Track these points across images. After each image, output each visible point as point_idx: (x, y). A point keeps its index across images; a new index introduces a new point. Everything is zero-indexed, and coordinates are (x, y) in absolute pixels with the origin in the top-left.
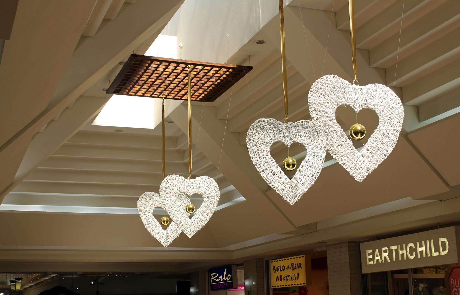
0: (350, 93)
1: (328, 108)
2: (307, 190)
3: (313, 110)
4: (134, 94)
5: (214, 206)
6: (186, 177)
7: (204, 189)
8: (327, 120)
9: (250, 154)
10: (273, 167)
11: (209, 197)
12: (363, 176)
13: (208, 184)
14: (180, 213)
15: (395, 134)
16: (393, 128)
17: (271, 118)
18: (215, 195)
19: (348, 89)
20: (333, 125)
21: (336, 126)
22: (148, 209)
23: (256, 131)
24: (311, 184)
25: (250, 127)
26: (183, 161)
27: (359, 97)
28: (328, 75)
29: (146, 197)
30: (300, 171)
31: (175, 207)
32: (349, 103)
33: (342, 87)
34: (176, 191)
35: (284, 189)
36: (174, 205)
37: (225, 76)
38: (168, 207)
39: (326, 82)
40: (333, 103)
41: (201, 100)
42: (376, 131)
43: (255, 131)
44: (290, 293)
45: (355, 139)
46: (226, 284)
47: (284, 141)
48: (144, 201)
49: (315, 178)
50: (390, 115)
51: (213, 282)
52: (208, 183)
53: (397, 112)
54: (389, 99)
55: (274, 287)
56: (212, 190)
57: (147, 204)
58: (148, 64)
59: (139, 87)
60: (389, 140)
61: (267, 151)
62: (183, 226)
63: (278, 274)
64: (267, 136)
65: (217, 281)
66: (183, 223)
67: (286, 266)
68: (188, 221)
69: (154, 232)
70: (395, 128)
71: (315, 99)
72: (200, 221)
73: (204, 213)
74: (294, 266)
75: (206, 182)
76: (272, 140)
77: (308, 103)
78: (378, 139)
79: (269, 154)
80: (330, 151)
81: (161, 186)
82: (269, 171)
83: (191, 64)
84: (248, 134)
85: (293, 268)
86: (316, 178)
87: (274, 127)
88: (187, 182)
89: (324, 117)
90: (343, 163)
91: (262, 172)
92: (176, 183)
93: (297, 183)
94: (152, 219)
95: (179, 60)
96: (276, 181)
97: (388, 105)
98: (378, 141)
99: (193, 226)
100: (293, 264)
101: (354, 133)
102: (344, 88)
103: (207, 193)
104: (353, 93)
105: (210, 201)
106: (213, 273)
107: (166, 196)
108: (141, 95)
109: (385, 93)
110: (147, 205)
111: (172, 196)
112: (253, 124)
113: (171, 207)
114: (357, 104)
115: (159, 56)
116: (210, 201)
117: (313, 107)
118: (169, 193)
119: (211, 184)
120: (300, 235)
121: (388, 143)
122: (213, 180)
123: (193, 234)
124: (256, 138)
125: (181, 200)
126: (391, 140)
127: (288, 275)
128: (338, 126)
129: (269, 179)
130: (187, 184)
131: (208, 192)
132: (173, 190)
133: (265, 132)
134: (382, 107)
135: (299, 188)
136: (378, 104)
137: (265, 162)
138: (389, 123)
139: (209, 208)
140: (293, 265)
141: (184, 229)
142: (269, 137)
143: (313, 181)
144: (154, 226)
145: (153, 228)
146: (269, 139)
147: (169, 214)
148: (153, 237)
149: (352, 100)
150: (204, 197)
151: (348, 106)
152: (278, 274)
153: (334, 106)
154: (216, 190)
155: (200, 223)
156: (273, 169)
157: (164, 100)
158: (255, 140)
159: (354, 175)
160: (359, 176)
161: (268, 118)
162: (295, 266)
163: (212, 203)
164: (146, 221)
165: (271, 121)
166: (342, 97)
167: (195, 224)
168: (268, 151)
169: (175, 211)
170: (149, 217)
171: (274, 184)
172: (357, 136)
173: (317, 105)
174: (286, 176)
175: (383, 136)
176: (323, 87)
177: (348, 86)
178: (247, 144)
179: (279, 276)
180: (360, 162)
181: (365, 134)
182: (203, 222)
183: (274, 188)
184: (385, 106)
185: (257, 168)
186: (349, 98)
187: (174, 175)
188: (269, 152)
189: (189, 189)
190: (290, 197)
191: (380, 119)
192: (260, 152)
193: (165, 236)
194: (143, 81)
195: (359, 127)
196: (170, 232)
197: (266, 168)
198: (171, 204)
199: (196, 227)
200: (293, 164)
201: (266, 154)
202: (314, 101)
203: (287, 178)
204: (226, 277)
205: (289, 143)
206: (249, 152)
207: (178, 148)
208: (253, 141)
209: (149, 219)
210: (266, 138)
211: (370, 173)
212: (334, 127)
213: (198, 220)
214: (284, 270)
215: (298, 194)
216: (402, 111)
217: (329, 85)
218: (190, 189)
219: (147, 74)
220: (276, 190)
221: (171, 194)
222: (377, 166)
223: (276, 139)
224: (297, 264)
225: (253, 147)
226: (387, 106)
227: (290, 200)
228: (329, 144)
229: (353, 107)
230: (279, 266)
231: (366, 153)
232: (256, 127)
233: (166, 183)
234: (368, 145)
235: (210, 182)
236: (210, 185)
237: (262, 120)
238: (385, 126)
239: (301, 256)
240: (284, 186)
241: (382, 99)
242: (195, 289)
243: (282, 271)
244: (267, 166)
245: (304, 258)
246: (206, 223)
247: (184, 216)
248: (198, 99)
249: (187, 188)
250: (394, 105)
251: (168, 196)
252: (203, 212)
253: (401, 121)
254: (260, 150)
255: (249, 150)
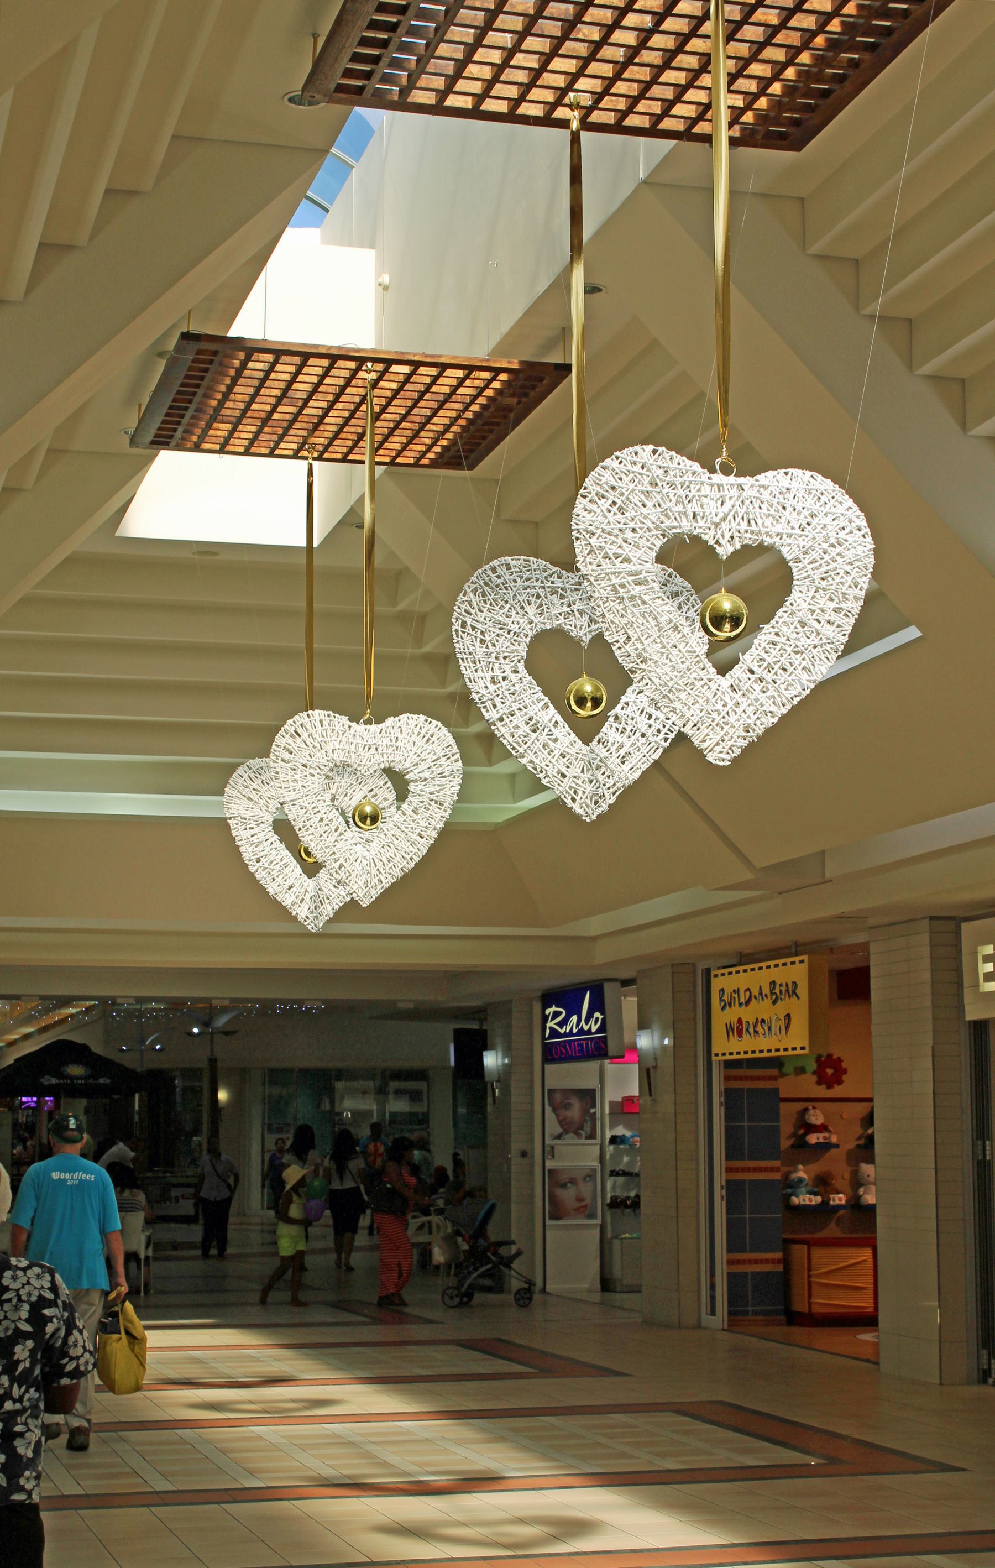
0: (705, 500)
1: (631, 546)
2: (637, 775)
3: (586, 552)
4: (217, 447)
5: (443, 808)
6: (355, 718)
7: (411, 754)
8: (628, 583)
9: (464, 669)
10: (534, 707)
11: (425, 780)
12: (730, 748)
13: (426, 739)
14: (333, 829)
15: (840, 623)
16: (833, 605)
17: (531, 559)
18: (446, 774)
19: (698, 487)
20: (646, 598)
21: (657, 600)
22: (257, 811)
23: (481, 598)
24: (650, 759)
25: (466, 587)
26: (420, 648)
27: (730, 511)
28: (637, 448)
29: (252, 775)
30: (617, 718)
31: (319, 812)
32: (701, 531)
33: (681, 483)
34: (321, 760)
35: (566, 773)
36: (314, 805)
37: (489, 393)
38: (294, 809)
39: (630, 467)
40: (649, 531)
41: (434, 464)
42: (780, 613)
43: (478, 599)
44: (783, 1075)
45: (716, 638)
46: (587, 1044)
47: (569, 627)
48: (247, 787)
49: (666, 740)
50: (828, 564)
51: (550, 1037)
52: (424, 736)
53: (850, 555)
54: (830, 515)
55: (728, 1057)
56: (435, 758)
57: (254, 796)
58: (238, 362)
59: (229, 427)
60: (817, 642)
61: (516, 658)
62: (343, 868)
63: (732, 1015)
64: (517, 613)
65: (562, 1031)
66: (342, 860)
67: (755, 992)
68: (359, 854)
69: (277, 884)
70: (843, 605)
71: (594, 518)
72: (397, 854)
73: (410, 829)
74: (777, 991)
75: (419, 733)
76: (534, 625)
77: (573, 530)
78: (783, 640)
79: (521, 667)
80: (636, 675)
81: (274, 747)
82: (519, 719)
83: (375, 360)
84: (459, 608)
85: (774, 997)
86: (669, 741)
87: (539, 584)
88: (357, 734)
89: (620, 573)
90: (671, 709)
91: (499, 724)
92: (323, 736)
93: (607, 754)
94: (272, 843)
95: (331, 347)
96: (540, 751)
97: (822, 535)
98: (785, 644)
99: (374, 871)
100: (773, 983)
101: (710, 619)
102: (687, 483)
103: (420, 768)
104: (711, 499)
105: (431, 793)
106: (551, 1007)
107: (289, 778)
108: (242, 449)
109: (816, 498)
110: (255, 798)
111: (309, 778)
112: (475, 575)
113: (304, 811)
114: (723, 532)
115: (269, 338)
116: (431, 793)
117: (586, 545)
118: (300, 766)
119: (434, 739)
120: (780, 893)
121: (815, 651)
122: (440, 725)
123: (375, 894)
124: (482, 620)
125: (362, 784)
126: (824, 641)
127: (759, 1020)
128: (663, 600)
129: (518, 743)
130: (358, 740)
131: (423, 766)
132: (314, 759)
133: (512, 602)
134: (804, 540)
135: (612, 771)
136: (793, 531)
137: (506, 693)
138: (824, 589)
139: (427, 815)
140: (774, 988)
141: (344, 878)
142: (524, 615)
143: (657, 748)
144: (278, 866)
145: (273, 870)
146: (521, 621)
147: (298, 832)
148: (275, 899)
149: (709, 521)
150: (412, 781)
151: (696, 539)
152: (732, 1015)
153: (652, 539)
154: (449, 758)
155: (396, 862)
156: (532, 714)
157: (311, 465)
158: (479, 626)
159: (704, 745)
160: (718, 749)
161: (522, 557)
162: (781, 991)
163: (435, 799)
164: (250, 850)
165: (530, 566)
166: (676, 514)
167: (380, 865)
168: (519, 658)
169: (318, 825)
170: (261, 836)
171: (534, 759)
172: (720, 630)
173: (598, 538)
174: (573, 735)
175: (800, 629)
176: (620, 484)
177: (698, 479)
178: (455, 636)
179: (736, 1022)
180: (724, 706)
181: (744, 623)
182: (408, 857)
183: (535, 769)
184: (814, 538)
185: (483, 711)
186: (701, 514)
187: (317, 712)
188: (522, 662)
189: (363, 754)
190: (584, 797)
191: (795, 578)
192: (495, 661)
193: (311, 898)
194: (238, 411)
195: (727, 603)
196: (329, 884)
197: (511, 709)
198: (306, 802)
199: (383, 872)
200: (596, 698)
201: (512, 667)
202: (591, 525)
203: (576, 739)
204: (587, 1022)
205: (586, 634)
206: (460, 661)
207: (401, 606)
208: (473, 628)
209: (261, 842)
210: (515, 617)
211: (753, 741)
212: (650, 602)
213: (390, 851)
214: (748, 1002)
215: (609, 788)
216: (867, 553)
217: (640, 477)
218: (367, 755)
219: (243, 390)
220: (541, 776)
221: (307, 769)
222: (776, 720)
223: (546, 621)
224: (787, 985)
225: (471, 648)
226: (819, 537)
227: (584, 805)
228: (631, 653)
229: (711, 542)
230: (734, 991)
231: (743, 681)
232: (482, 584)
233: (292, 736)
234: (752, 658)
235: (430, 733)
236: (431, 742)
237: (502, 565)
238: (808, 600)
239: (797, 959)
240: (565, 764)
241: (806, 517)
242: (500, 1056)
243: (744, 1007)
244: (513, 704)
245: (805, 966)
246: (417, 859)
247: (346, 840)
248: (425, 461)
249: (358, 753)
250: (842, 535)
251: (296, 777)
252: (407, 828)
253: (862, 583)
254: (493, 655)
255: (458, 655)
